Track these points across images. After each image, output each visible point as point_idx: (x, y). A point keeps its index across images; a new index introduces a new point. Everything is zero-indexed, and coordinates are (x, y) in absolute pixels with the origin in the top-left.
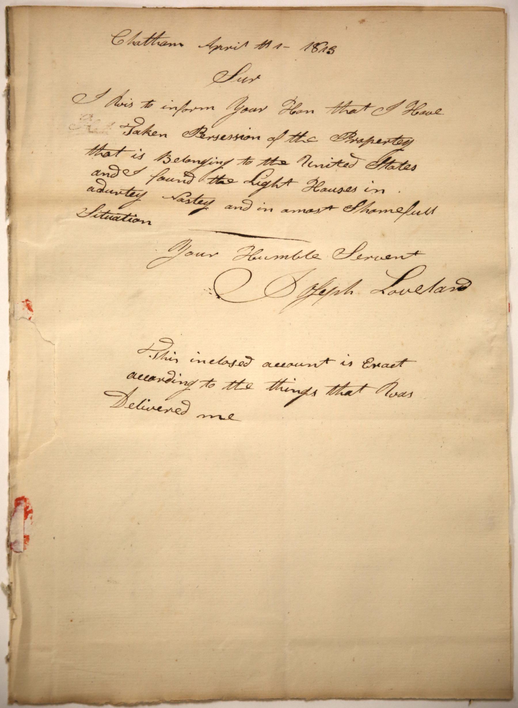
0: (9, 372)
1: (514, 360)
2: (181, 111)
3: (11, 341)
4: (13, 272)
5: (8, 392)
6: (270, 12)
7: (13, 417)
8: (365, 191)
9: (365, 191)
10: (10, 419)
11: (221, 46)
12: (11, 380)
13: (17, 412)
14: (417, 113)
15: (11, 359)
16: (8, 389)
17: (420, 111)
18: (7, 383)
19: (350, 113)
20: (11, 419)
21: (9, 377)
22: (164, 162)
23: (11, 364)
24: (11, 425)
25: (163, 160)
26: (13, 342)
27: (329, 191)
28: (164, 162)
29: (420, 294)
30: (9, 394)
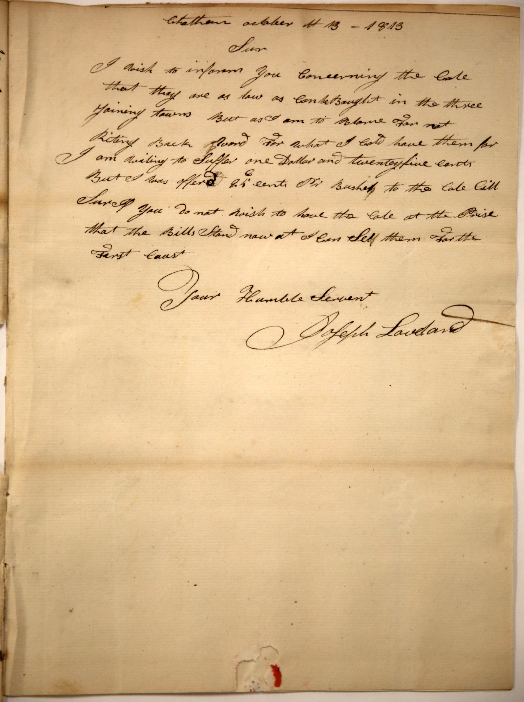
0: (6, 378)
1: (520, 414)
2: (207, 73)
3: (7, 346)
4: (6, 281)
5: (4, 399)
6: (89, 693)
7: (9, 425)
8: (242, 69)
9: (242, 69)
10: (6, 426)
11: (405, 143)
12: (8, 386)
13: (13, 419)
14: (304, 77)
15: (8, 365)
16: (4, 396)
17: (306, 75)
18: (4, 387)
19: (402, 145)
20: (7, 426)
21: (6, 384)
22: (157, 146)
23: (8, 370)
24: (7, 431)
25: (156, 144)
26: (10, 346)
27: (253, 98)
28: (157, 146)
29: (311, 178)
30: (6, 400)
